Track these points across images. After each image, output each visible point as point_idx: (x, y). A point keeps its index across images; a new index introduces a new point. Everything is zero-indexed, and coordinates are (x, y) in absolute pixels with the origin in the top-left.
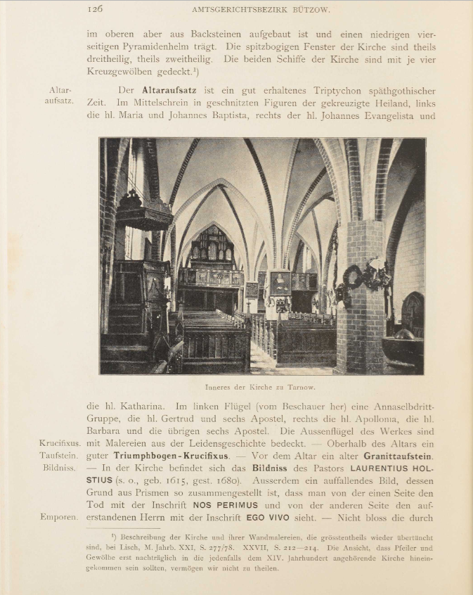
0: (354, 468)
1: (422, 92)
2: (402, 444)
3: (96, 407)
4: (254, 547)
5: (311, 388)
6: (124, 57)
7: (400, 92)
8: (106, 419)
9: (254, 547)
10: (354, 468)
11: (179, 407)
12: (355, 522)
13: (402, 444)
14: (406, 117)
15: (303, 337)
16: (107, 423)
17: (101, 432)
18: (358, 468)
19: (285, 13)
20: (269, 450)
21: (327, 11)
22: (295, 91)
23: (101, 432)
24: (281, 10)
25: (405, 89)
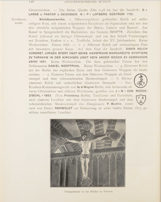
0: (30, 14)
1: (113, 19)
2: (61, 24)
3: (63, 10)
4: (112, 40)
5: (111, 192)
6: (101, 86)
7: (105, 20)
8: (79, 28)
9: (112, 40)
10: (30, 14)
11: (128, 10)
12: (66, 114)
13: (61, 24)
14: (129, 10)
15: (81, 155)
16: (79, 29)
17: (96, 41)
18: (31, 14)
19: (96, 3)
20: (102, 47)
21: (73, 41)
22: (45, 113)
23: (96, 41)
24: (95, 2)
25: (107, 19)
